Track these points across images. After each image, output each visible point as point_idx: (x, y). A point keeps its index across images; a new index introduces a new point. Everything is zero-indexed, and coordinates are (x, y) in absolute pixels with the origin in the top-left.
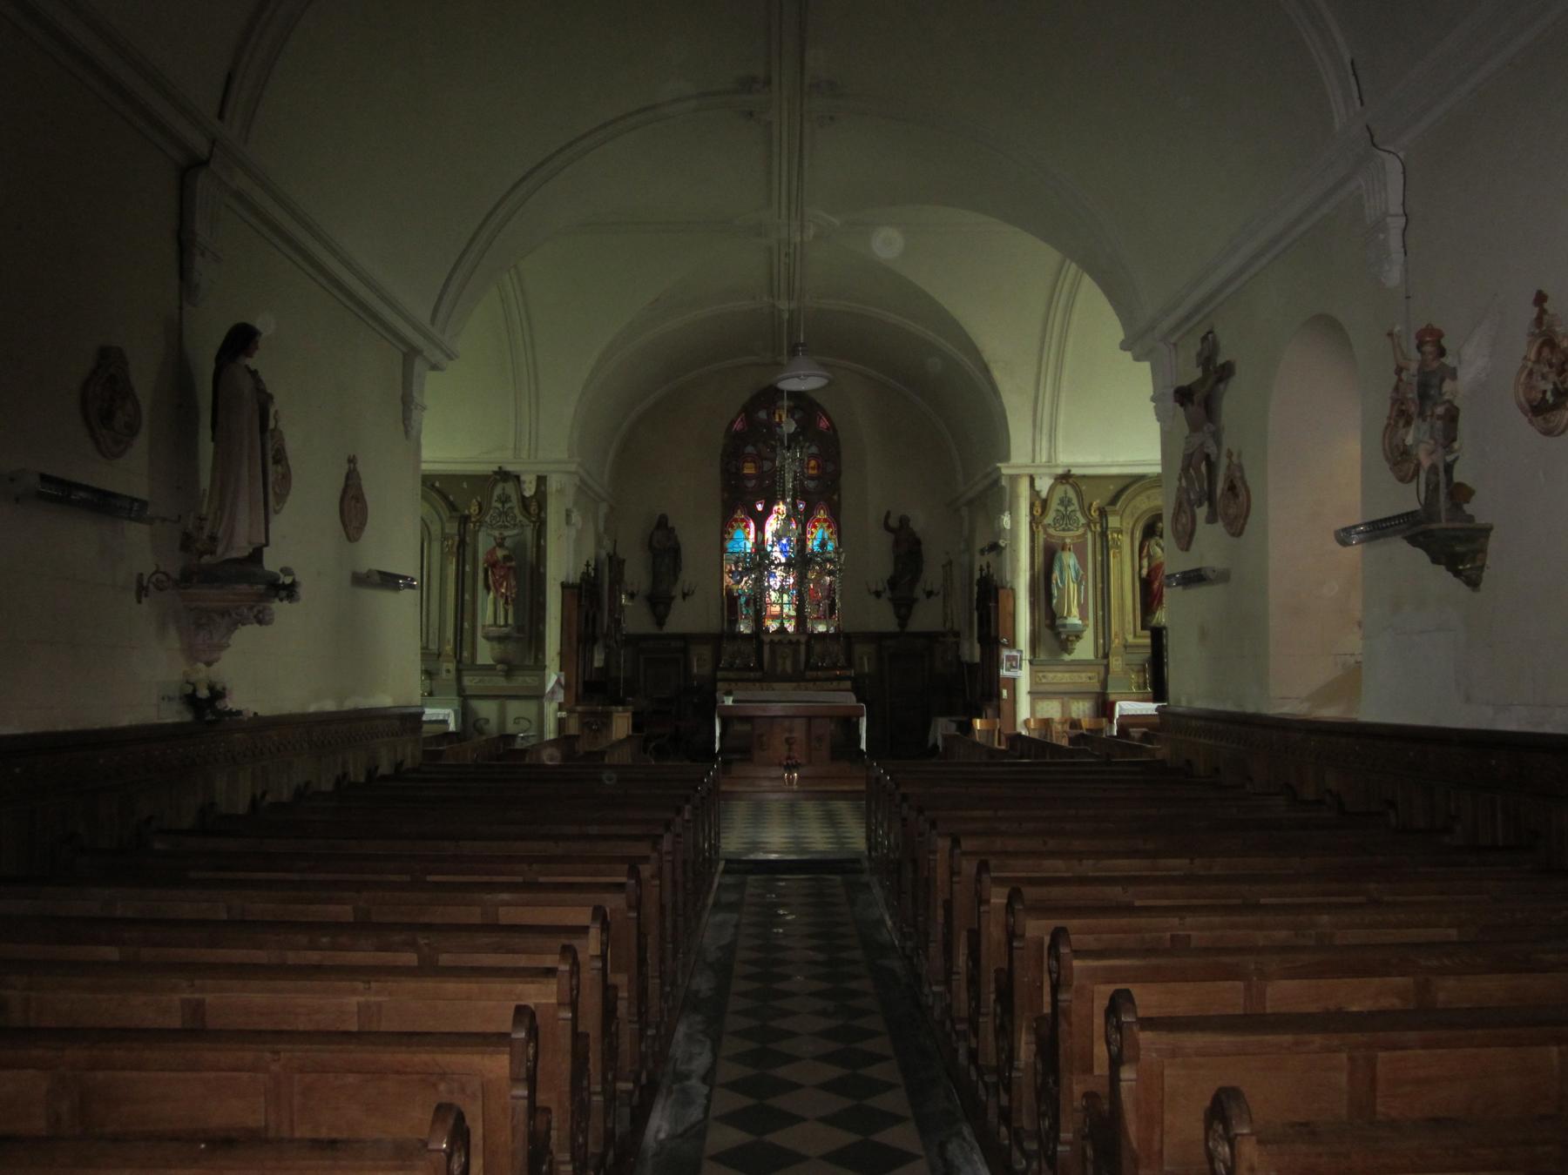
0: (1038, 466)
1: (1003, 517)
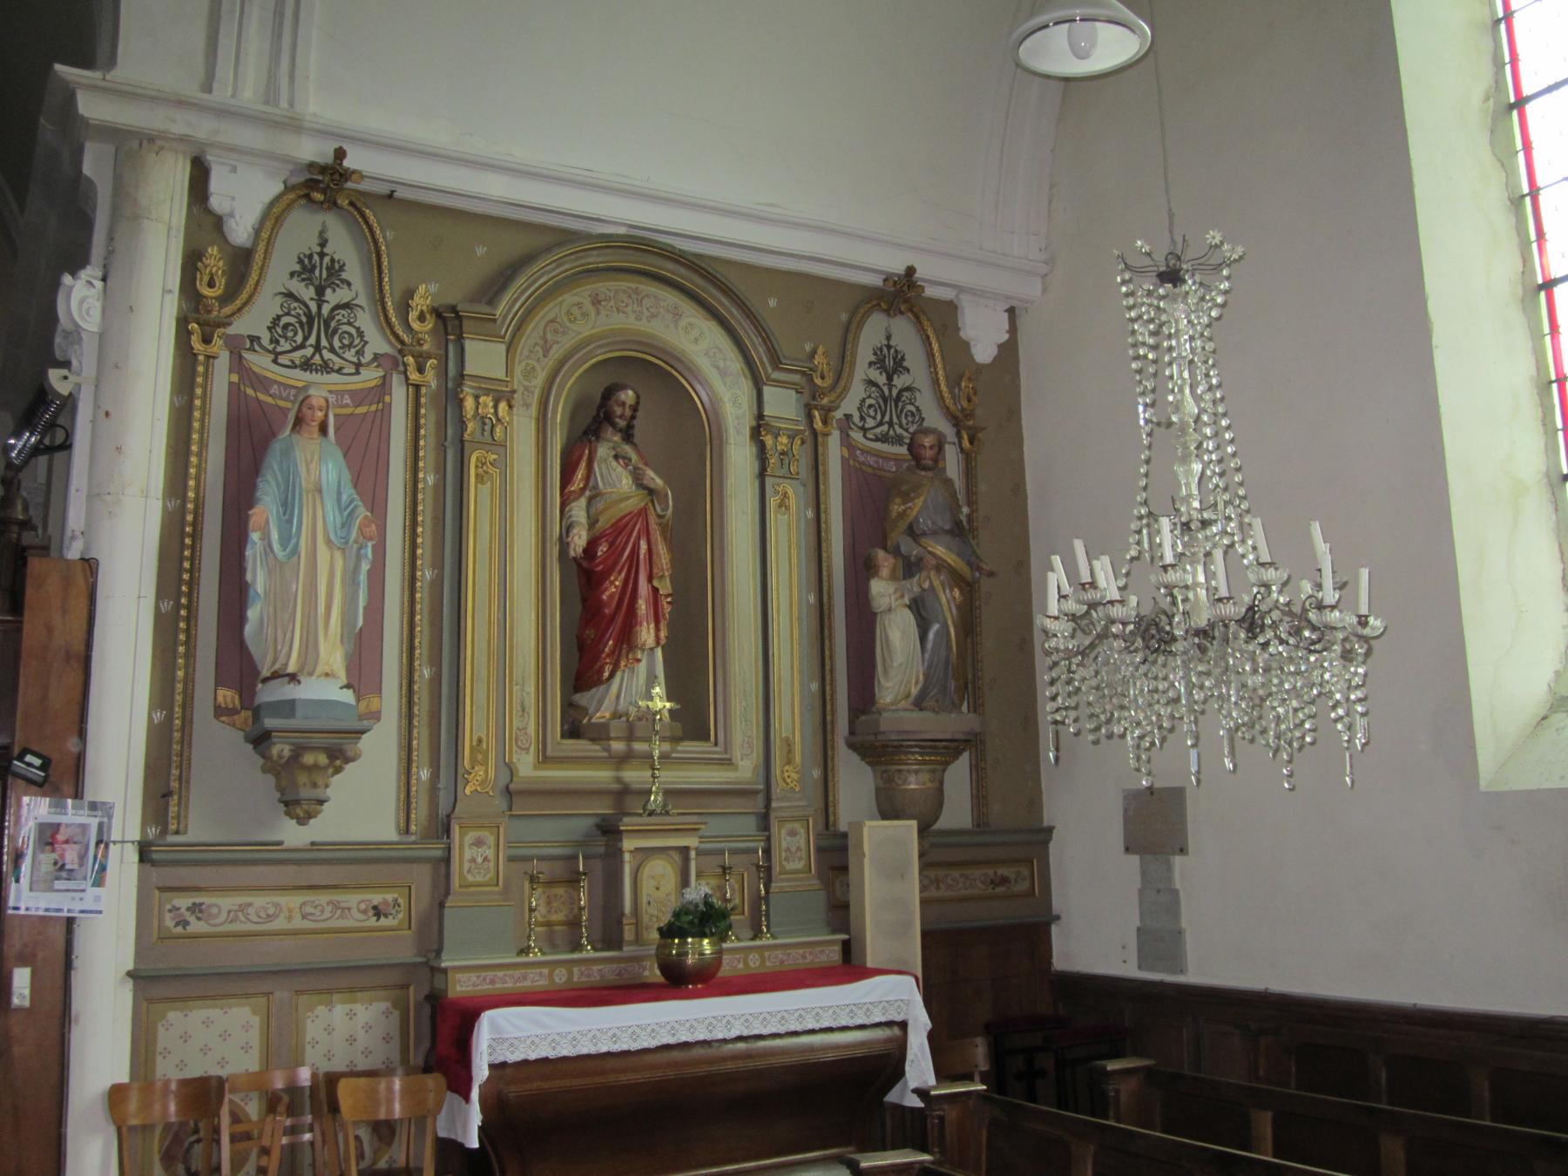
0: (223, 113)
1: (67, 279)
